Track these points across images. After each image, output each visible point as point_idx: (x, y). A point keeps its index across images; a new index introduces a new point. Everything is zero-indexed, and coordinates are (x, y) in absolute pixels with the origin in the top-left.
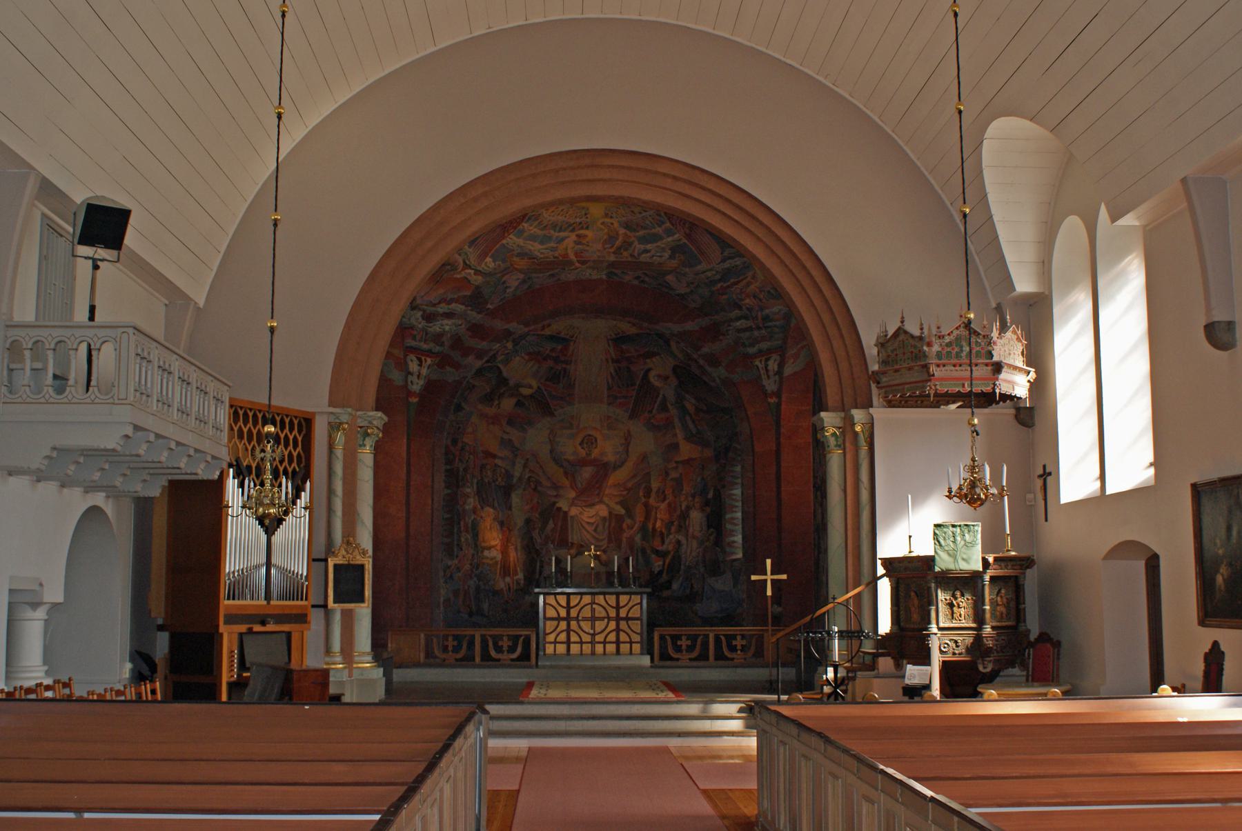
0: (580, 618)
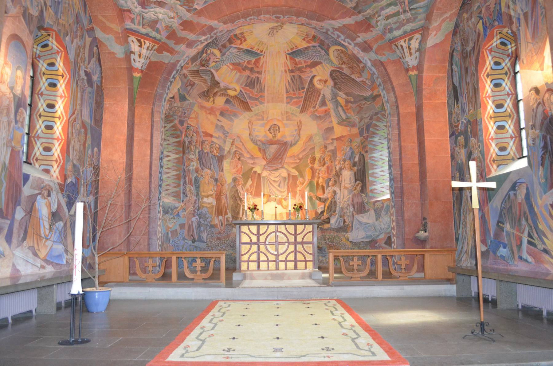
0: (267, 243)
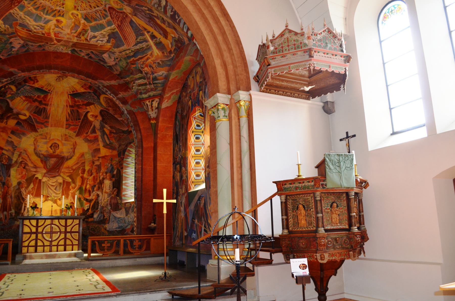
0: (44, 232)
